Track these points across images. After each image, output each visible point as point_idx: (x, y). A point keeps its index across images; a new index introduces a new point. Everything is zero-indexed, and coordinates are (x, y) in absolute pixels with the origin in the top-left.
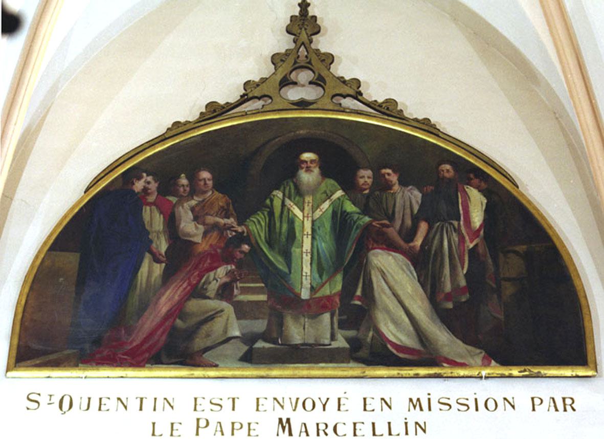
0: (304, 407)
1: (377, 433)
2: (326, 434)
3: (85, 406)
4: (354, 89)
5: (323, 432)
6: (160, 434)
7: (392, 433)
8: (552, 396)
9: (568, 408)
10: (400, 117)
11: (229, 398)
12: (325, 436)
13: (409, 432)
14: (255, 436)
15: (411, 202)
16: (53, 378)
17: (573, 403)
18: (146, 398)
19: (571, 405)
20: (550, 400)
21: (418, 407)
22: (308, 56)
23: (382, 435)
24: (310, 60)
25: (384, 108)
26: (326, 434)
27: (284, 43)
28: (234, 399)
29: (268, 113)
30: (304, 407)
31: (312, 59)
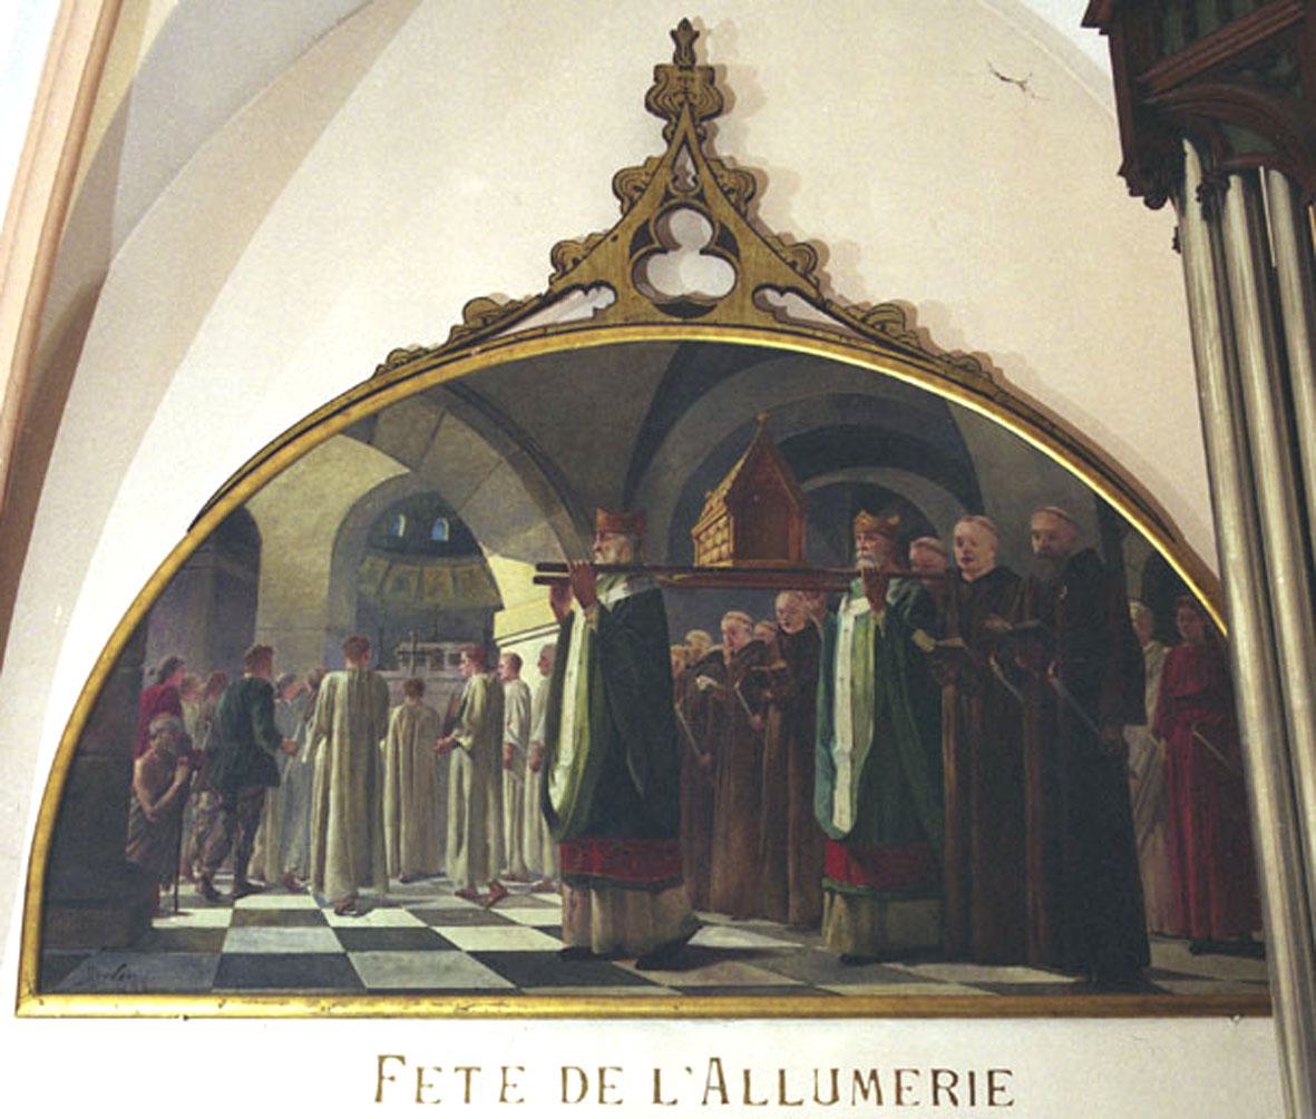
0: (583, 1077)
1: (788, 1099)
2: (954, 1101)
3: (826, 1095)
4: (805, 261)
5: (947, 1097)
6: (763, 1100)
7: (662, 1098)
8: (715, 1056)
9: (943, 1094)
10: (917, 352)
11: (457, 1070)
12: (951, 1104)
13: (471, 1098)
14: (1005, 1105)
15: (977, 985)
16: (393, 1056)
17: (954, 1084)
18: (479, 1069)
19: (948, 1089)
20: (711, 1066)
21: (873, 1094)
22: (698, 177)
23: (800, 1103)
24: (702, 190)
25: (873, 326)
26: (954, 1101)
27: (642, 141)
28: (468, 1071)
29: (74, 137)
30: (583, 1077)
31: (706, 187)
